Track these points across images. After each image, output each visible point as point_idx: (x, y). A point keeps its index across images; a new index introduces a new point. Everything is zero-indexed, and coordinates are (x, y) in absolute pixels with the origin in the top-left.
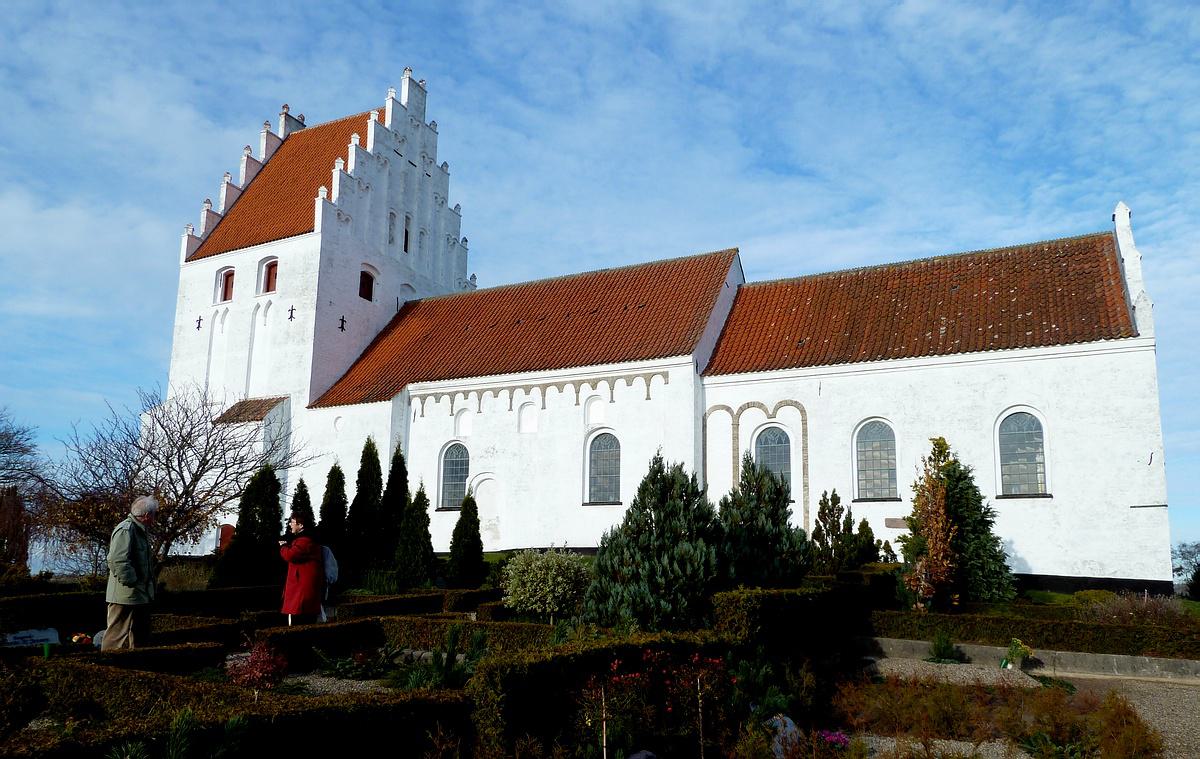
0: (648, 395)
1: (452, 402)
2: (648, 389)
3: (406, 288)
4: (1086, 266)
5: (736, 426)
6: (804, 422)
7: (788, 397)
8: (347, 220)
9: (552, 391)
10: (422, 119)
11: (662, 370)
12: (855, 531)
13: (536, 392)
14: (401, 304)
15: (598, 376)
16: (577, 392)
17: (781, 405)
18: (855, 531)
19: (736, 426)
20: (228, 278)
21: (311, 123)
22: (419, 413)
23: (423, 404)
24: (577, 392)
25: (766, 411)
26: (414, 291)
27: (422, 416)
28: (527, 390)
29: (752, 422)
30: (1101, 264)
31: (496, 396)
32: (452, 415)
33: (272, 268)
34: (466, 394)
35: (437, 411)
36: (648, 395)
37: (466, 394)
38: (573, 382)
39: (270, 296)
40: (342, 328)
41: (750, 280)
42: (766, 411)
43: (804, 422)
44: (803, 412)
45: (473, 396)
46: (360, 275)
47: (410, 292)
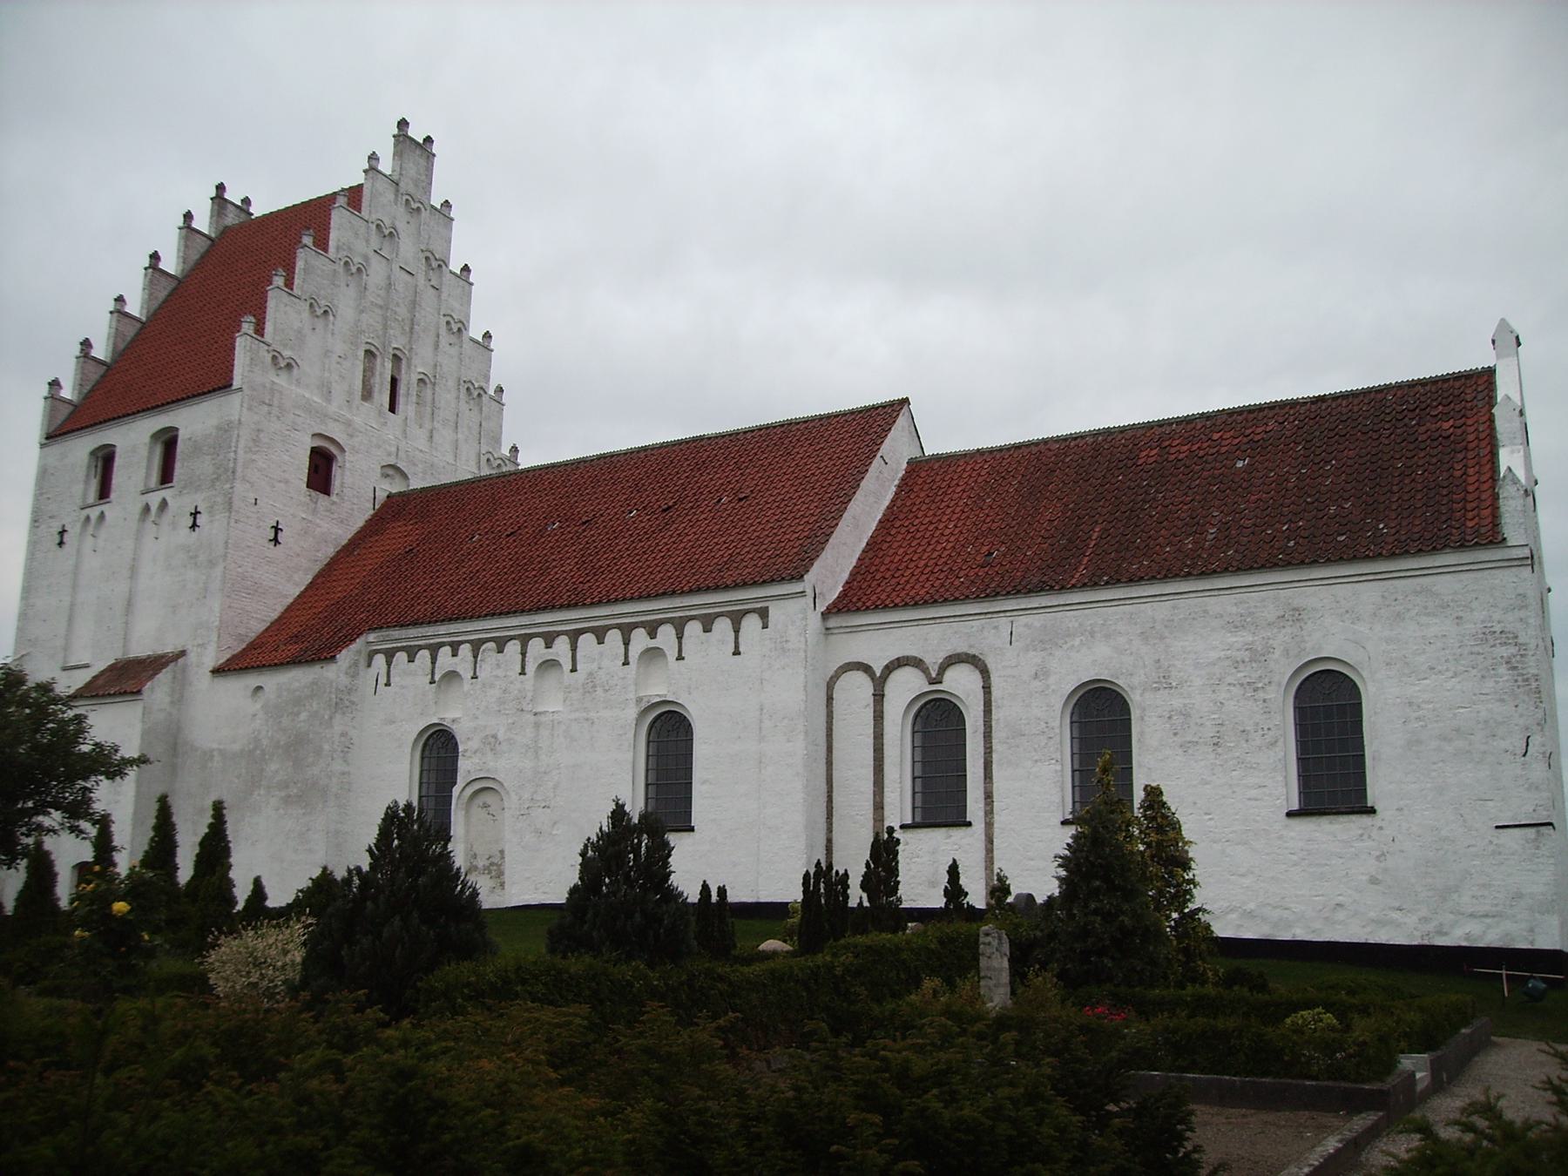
0: (475, 673)
1: (434, 662)
2: (737, 638)
3: (391, 472)
4: (1446, 425)
5: (879, 697)
6: (987, 689)
7: (962, 648)
8: (289, 366)
9: (587, 641)
10: (424, 199)
11: (759, 605)
12: (714, 898)
13: (562, 644)
14: (382, 496)
15: (508, 633)
16: (626, 643)
17: (953, 660)
18: (714, 898)
19: (879, 697)
20: (105, 460)
21: (257, 211)
22: (382, 680)
23: (389, 664)
24: (626, 643)
25: (925, 671)
26: (404, 476)
27: (388, 684)
28: (549, 639)
29: (906, 688)
30: (1470, 422)
31: (500, 651)
32: (432, 682)
33: (168, 442)
34: (455, 647)
35: (412, 675)
36: (475, 673)
37: (455, 647)
38: (619, 626)
39: (166, 493)
40: (276, 541)
41: (935, 445)
42: (925, 671)
43: (987, 689)
44: (985, 673)
45: (465, 650)
46: (309, 452)
47: (398, 478)
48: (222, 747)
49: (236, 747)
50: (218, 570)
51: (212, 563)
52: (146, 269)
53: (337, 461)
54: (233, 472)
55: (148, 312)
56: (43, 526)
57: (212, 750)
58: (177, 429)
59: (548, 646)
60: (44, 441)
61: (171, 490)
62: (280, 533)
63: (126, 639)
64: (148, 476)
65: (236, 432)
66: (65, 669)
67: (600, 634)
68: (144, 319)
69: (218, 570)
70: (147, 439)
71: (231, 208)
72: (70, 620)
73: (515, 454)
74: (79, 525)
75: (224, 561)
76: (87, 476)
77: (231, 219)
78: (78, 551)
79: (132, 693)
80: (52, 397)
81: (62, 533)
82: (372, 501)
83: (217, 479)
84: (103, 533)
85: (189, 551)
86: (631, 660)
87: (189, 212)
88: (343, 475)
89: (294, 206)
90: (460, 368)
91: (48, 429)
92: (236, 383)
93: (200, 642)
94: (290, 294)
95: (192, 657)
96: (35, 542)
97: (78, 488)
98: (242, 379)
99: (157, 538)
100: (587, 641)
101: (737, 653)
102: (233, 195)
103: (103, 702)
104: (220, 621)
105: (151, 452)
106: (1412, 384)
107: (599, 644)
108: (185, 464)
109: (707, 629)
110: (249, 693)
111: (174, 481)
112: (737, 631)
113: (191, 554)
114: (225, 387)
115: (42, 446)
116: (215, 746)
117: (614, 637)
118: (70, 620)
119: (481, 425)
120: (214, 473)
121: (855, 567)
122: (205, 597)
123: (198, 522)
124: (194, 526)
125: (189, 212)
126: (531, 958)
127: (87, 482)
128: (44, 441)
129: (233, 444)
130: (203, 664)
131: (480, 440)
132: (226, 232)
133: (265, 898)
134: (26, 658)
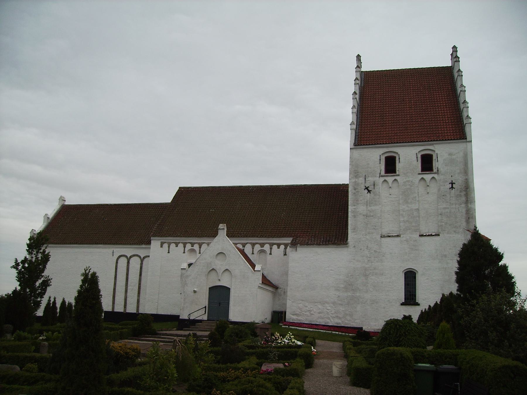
16: (185, 247)
24: (185, 247)
28: (192, 244)
59: (192, 246)
60: (353, 147)
62: (368, 188)
67: (279, 245)
86: (185, 251)
87: (358, 55)
100: (275, 247)
101: (169, 252)
103: (116, 246)
106: (189, 188)
107: (278, 248)
109: (177, 246)
112: (253, 249)
117: (181, 246)
125: (358, 55)
126: (369, 391)
128: (353, 147)
133: (13, 266)
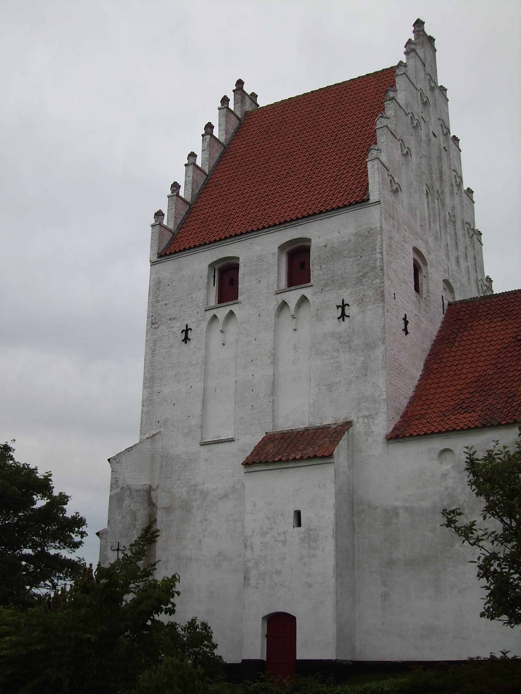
48: (407, 505)
49: (426, 504)
50: (379, 352)
51: (369, 346)
52: (203, 136)
53: (422, 272)
54: (382, 269)
55: (209, 168)
56: (162, 327)
57: (395, 510)
58: (309, 240)
61: (310, 288)
63: (274, 418)
64: (279, 280)
65: (379, 237)
66: (203, 444)
68: (206, 170)
69: (379, 352)
70: (276, 250)
71: (246, 96)
72: (204, 402)
73: (490, 283)
74: (204, 325)
75: (383, 343)
76: (208, 283)
77: (248, 107)
78: (207, 345)
79: (323, 457)
80: (159, 224)
81: (187, 331)
82: (442, 306)
83: (364, 276)
84: (232, 329)
85: (340, 337)
88: (428, 283)
89: (312, 92)
90: (463, 212)
91: (159, 249)
92: (374, 195)
93: (367, 413)
94: (419, 122)
95: (359, 427)
96: (155, 340)
97: (200, 295)
98: (379, 194)
99: (295, 330)
102: (248, 89)
103: (326, 462)
104: (387, 394)
105: (279, 260)
108: (324, 266)
110: (435, 456)
111: (312, 281)
113: (342, 340)
114: (363, 201)
115: (153, 263)
116: (398, 504)
118: (204, 402)
119: (475, 258)
120: (359, 272)
121: (398, 422)
122: (366, 375)
123: (347, 313)
124: (343, 316)
127: (208, 288)
129: (378, 247)
130: (373, 432)
131: (476, 269)
132: (247, 114)
134: (157, 437)
